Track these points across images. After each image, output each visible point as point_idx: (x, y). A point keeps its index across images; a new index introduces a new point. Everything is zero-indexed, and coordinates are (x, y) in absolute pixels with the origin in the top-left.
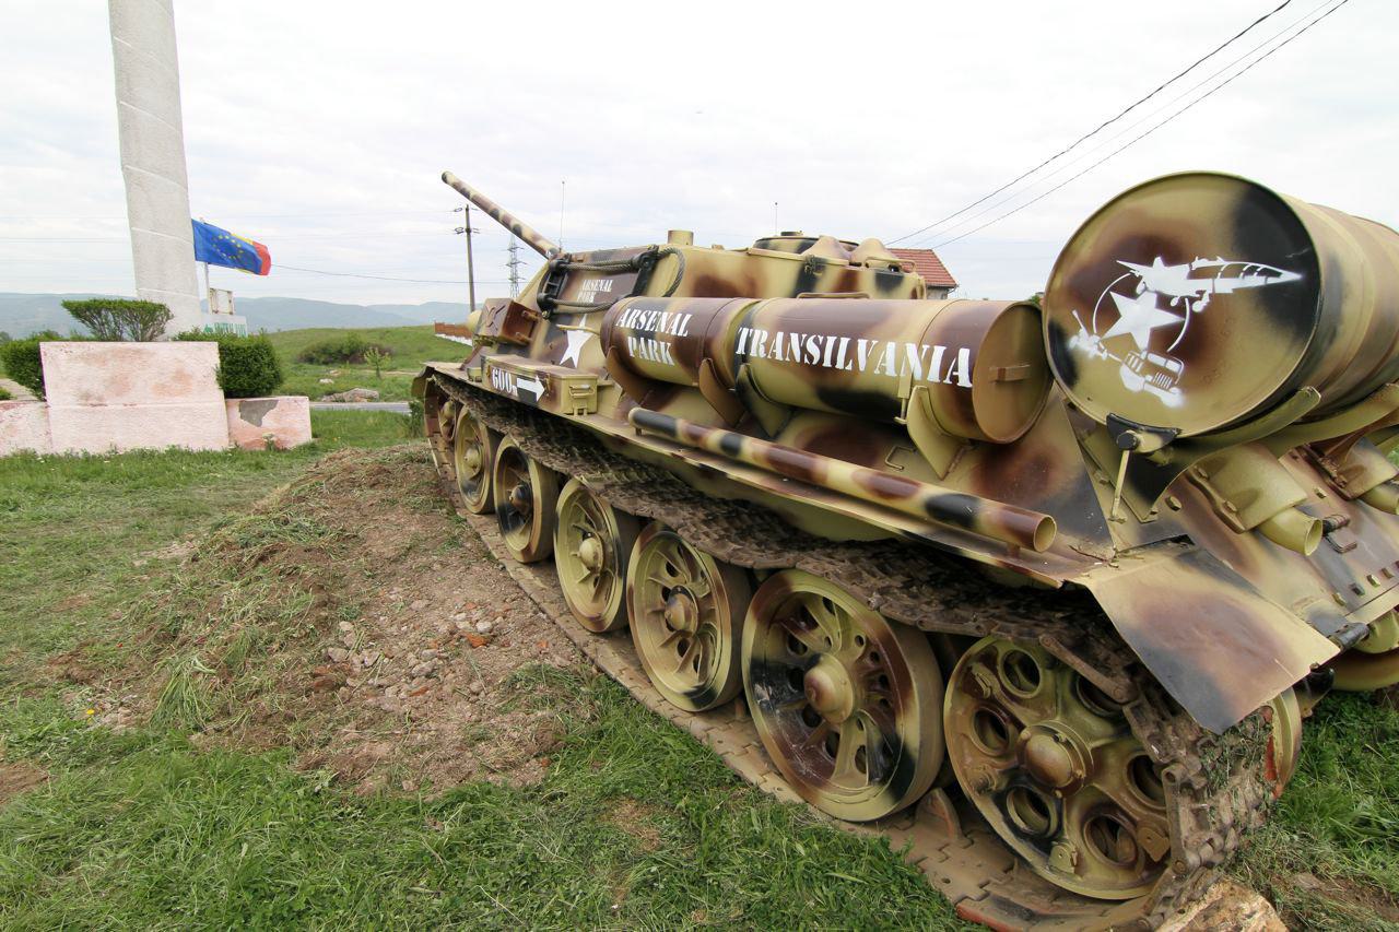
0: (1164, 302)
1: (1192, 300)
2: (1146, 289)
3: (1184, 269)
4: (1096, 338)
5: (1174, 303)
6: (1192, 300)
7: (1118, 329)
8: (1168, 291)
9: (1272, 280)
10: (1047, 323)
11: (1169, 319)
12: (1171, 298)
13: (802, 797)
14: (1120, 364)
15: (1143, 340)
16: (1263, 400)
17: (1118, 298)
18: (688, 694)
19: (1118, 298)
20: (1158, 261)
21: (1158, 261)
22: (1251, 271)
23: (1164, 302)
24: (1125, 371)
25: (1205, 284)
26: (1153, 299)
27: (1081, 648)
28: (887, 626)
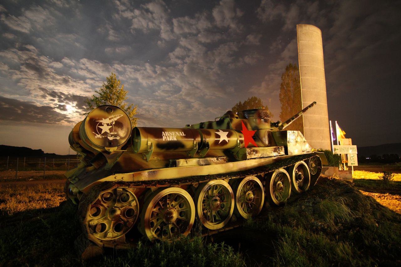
0: (108, 125)
1: (112, 123)
2: (104, 124)
3: (108, 119)
4: (100, 135)
5: (110, 124)
6: (112, 123)
7: (103, 132)
8: (108, 123)
9: (121, 116)
10: (88, 226)
11: (110, 127)
12: (109, 124)
13: (116, 146)
14: (107, 137)
15: (108, 132)
16: (154, 198)
17: (100, 127)
18: (281, 113)
19: (100, 127)
20: (103, 119)
21: (103, 119)
22: (118, 116)
23: (108, 125)
24: (109, 138)
25: (112, 120)
26: (106, 125)
27: (33, 166)
28: (272, 147)
